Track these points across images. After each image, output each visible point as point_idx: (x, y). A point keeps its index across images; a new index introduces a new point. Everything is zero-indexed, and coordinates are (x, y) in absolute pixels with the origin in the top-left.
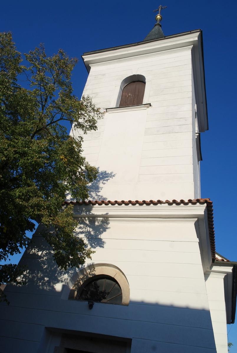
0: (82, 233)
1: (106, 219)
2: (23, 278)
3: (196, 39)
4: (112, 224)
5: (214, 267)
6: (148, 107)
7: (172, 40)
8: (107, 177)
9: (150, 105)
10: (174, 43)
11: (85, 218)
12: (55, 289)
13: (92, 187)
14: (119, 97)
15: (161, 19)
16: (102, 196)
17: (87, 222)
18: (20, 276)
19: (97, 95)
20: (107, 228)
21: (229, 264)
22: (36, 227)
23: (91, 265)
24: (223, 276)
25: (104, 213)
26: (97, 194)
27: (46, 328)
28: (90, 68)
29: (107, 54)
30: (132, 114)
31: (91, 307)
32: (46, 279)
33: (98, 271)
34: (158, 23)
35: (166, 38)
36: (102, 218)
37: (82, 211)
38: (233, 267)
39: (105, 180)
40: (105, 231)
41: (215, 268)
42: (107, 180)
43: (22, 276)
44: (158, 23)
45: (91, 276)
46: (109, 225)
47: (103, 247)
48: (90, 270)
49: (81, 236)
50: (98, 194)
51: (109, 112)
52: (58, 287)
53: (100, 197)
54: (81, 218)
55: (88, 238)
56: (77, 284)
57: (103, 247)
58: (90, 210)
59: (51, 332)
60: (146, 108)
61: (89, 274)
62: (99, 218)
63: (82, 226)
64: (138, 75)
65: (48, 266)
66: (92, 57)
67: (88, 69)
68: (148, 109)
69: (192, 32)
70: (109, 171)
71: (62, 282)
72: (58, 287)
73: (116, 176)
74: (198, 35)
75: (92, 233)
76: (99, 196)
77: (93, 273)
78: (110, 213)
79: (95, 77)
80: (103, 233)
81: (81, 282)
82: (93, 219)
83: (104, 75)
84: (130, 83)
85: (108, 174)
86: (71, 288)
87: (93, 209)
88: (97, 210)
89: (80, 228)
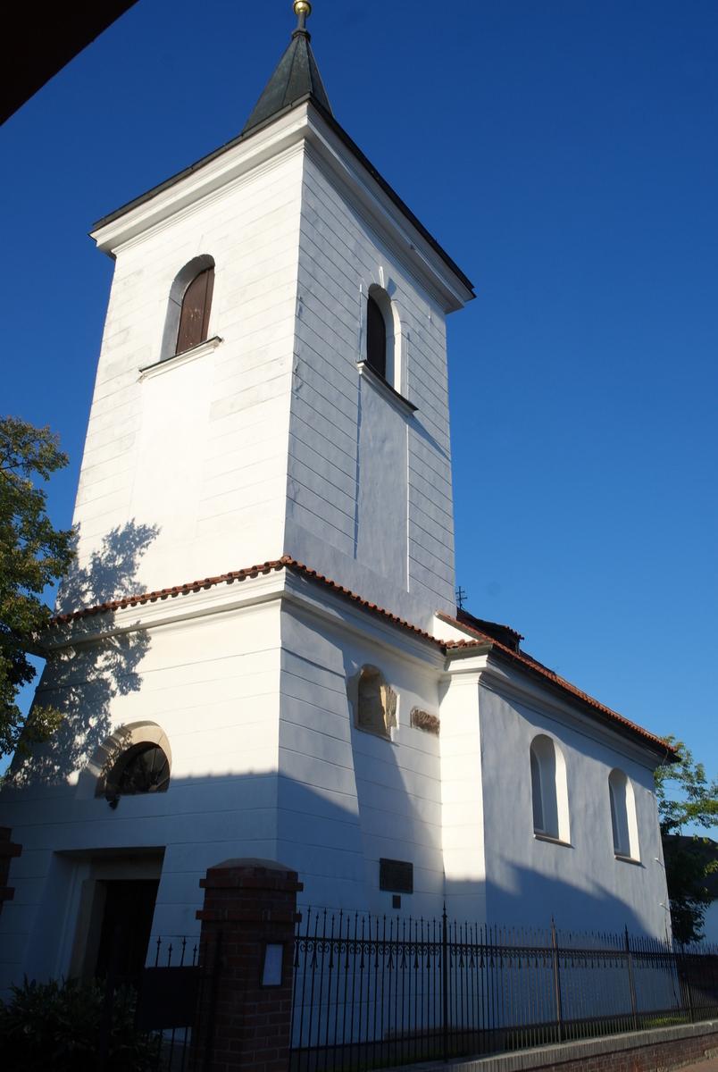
0: (107, 668)
1: (143, 633)
2: (24, 774)
3: (305, 121)
4: (157, 640)
5: (452, 662)
6: (216, 346)
7: (269, 134)
8: (147, 538)
9: (221, 340)
10: (262, 147)
11: (110, 637)
12: (68, 783)
13: (123, 567)
14: (168, 328)
15: (310, 8)
16: (139, 584)
17: (117, 644)
18: (19, 770)
19: (128, 333)
20: (146, 650)
21: (456, 654)
22: (40, 671)
23: (119, 729)
24: (476, 678)
25: (133, 622)
26: (130, 580)
27: (55, 852)
28: (114, 257)
29: (137, 215)
30: (198, 363)
31: (114, 805)
32: (56, 768)
33: (136, 738)
34: (300, 27)
35: (245, 135)
36: (135, 633)
37: (101, 625)
38: (487, 656)
39: (144, 546)
40: (143, 656)
41: (456, 665)
42: (147, 545)
43: (23, 770)
44: (297, 29)
45: (126, 749)
46: (151, 641)
47: (139, 689)
48: (125, 736)
49: (107, 675)
50: (134, 579)
51: (150, 376)
52: (73, 778)
53: (136, 586)
54: (105, 638)
55: (116, 677)
56: (107, 768)
57: (139, 689)
58: (111, 621)
59: (70, 858)
60: (212, 350)
61: (124, 745)
62: (131, 634)
63: (109, 653)
64: (203, 256)
65: (60, 744)
66: (111, 230)
67: (107, 258)
68: (217, 350)
69: (294, 104)
70: (150, 526)
71: (78, 768)
72: (73, 778)
73: (161, 533)
74: (306, 110)
75: (124, 665)
76: (135, 583)
77: (129, 741)
78: (144, 621)
79: (125, 284)
80: (139, 660)
81: (112, 762)
82: (123, 635)
83: (140, 272)
84: (198, 276)
85: (149, 530)
86: (99, 775)
87: (116, 617)
88: (124, 619)
89: (106, 658)
